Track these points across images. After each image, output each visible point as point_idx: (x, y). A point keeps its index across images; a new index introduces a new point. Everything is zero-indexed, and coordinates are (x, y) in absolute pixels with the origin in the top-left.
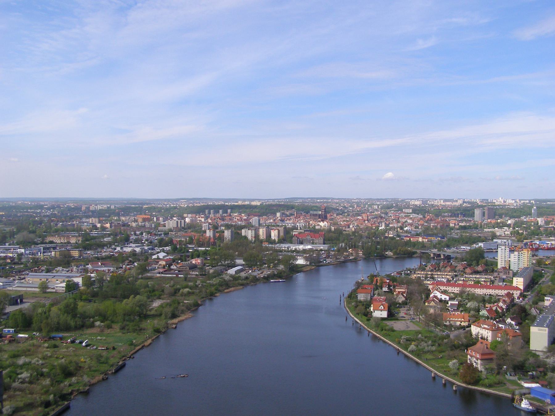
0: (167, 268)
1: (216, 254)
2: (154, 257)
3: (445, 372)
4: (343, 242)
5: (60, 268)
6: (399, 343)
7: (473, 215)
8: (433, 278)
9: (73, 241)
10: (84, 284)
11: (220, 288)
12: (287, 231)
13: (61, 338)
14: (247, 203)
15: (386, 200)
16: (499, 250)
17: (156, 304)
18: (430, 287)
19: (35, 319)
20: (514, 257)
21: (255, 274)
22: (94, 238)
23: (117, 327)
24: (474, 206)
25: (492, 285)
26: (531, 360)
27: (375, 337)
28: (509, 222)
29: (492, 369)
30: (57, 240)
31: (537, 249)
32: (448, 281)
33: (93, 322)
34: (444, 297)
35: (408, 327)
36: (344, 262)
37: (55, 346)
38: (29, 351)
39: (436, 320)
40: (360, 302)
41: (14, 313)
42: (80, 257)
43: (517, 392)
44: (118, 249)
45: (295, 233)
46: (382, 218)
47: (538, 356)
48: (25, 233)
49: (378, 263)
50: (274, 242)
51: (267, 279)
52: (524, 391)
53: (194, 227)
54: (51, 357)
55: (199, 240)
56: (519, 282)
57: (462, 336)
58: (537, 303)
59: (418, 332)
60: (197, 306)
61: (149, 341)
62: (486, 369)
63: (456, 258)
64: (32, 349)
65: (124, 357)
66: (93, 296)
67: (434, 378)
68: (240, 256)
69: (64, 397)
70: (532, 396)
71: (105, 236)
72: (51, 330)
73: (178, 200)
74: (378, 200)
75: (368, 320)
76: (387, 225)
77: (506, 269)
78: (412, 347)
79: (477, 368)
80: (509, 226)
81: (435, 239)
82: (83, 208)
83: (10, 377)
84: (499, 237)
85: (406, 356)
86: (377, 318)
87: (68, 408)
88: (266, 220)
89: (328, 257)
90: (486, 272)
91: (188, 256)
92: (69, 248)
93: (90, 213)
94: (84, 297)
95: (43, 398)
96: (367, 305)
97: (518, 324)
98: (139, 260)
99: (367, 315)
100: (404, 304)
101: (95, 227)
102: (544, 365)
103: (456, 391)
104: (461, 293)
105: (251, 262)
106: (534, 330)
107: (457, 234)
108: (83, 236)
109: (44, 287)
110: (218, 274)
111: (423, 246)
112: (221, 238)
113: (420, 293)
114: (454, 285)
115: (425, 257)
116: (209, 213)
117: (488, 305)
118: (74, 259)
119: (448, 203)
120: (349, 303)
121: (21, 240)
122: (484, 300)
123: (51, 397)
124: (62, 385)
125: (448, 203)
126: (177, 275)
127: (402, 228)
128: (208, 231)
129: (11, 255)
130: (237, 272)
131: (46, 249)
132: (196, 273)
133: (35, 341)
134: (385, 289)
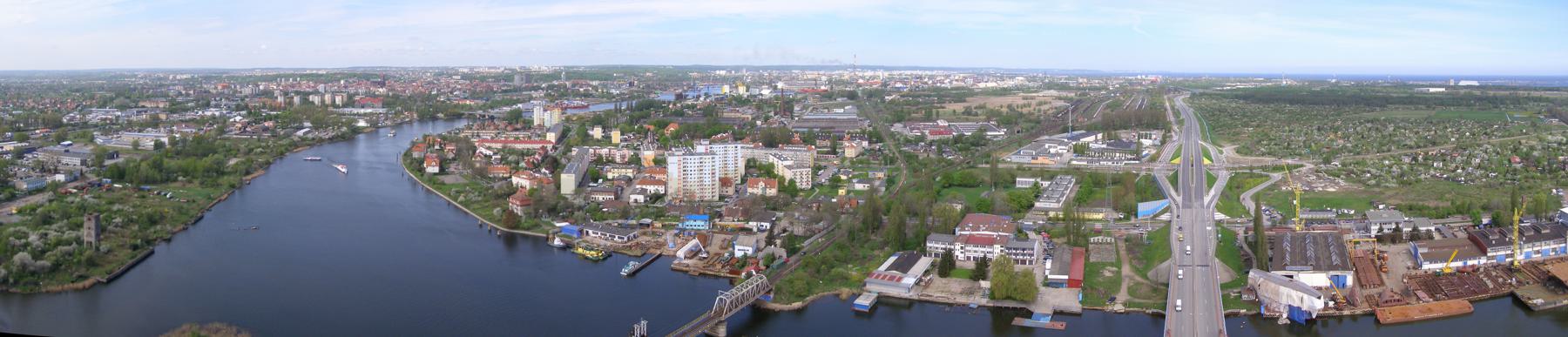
0: (243, 130)
1: (286, 117)
2: (232, 120)
3: (490, 220)
4: (400, 105)
5: (150, 129)
6: (449, 195)
7: (512, 80)
8: (478, 136)
9: (161, 105)
10: (170, 144)
11: (289, 148)
12: (350, 97)
13: (149, 190)
14: (314, 72)
15: (438, 68)
16: (535, 109)
17: (233, 162)
18: (477, 144)
19: (127, 172)
20: (547, 115)
21: (321, 135)
22: (179, 103)
23: (197, 182)
24: (514, 72)
25: (529, 140)
26: (562, 202)
27: (428, 190)
28: (543, 85)
29: (530, 213)
30: (148, 105)
31: (566, 108)
32: (492, 138)
33: (176, 178)
34: (489, 153)
35: (457, 180)
36: (401, 124)
37: (144, 197)
38: (122, 199)
39: (482, 173)
40: (415, 159)
41: (111, 167)
42: (167, 119)
43: (550, 232)
44: (200, 113)
45: (357, 98)
46: (434, 84)
47: (567, 199)
48: (122, 98)
49: (431, 124)
50: (338, 107)
51: (331, 140)
52: (556, 230)
53: (267, 93)
54: (139, 206)
55: (271, 105)
56: (551, 137)
57: (505, 186)
58: (566, 154)
59: (466, 185)
60: (268, 163)
61: (226, 195)
62: (525, 214)
63: (499, 118)
64: (125, 198)
65: (203, 210)
66: (177, 154)
67: (481, 226)
68: (308, 119)
69: (149, 242)
70: (563, 233)
71: (188, 102)
72: (141, 182)
73: (253, 70)
74: (431, 68)
75: (422, 175)
76: (438, 90)
77: (541, 126)
78: (461, 198)
79: (517, 214)
80: (543, 89)
81: (481, 102)
82: (171, 77)
83: (107, 221)
84: (535, 99)
85: (456, 207)
86: (430, 173)
87: (152, 253)
88: (98, 276)
89: (387, 119)
90: (524, 129)
91: (261, 120)
92: (158, 112)
93: (176, 82)
94: (169, 155)
95: (133, 241)
96: (421, 162)
97: (552, 172)
98: (218, 123)
99: (421, 171)
100: (454, 159)
101: (180, 94)
102: (572, 205)
103: (499, 236)
104: (504, 147)
105: (318, 125)
106: (563, 176)
107: (499, 97)
108: (170, 101)
109: (136, 145)
110: (287, 136)
111: (471, 108)
112: (291, 103)
113: (468, 150)
114: (497, 142)
115: (472, 117)
116: (281, 81)
117: (526, 158)
118: (162, 122)
119: (493, 70)
120: (404, 160)
121: (119, 104)
122: (522, 154)
123: (139, 241)
124: (148, 231)
125: (493, 70)
126: (252, 136)
127: (451, 93)
128: (279, 98)
129: (110, 117)
130: (305, 133)
131: (139, 113)
132: (266, 135)
133: (127, 191)
134: (437, 147)
